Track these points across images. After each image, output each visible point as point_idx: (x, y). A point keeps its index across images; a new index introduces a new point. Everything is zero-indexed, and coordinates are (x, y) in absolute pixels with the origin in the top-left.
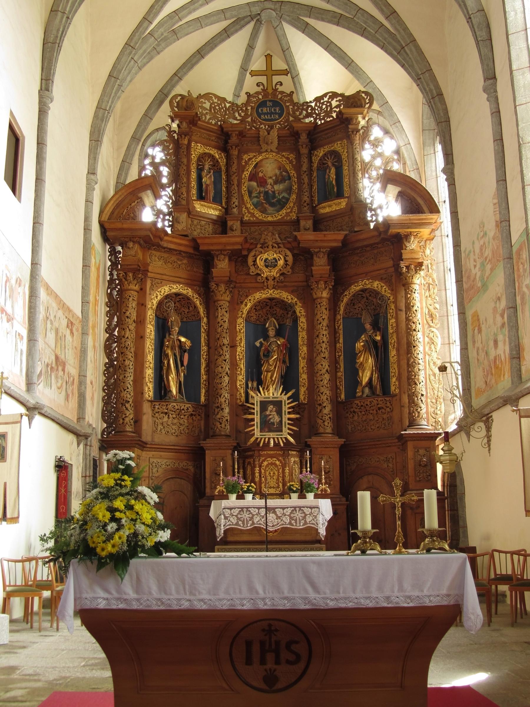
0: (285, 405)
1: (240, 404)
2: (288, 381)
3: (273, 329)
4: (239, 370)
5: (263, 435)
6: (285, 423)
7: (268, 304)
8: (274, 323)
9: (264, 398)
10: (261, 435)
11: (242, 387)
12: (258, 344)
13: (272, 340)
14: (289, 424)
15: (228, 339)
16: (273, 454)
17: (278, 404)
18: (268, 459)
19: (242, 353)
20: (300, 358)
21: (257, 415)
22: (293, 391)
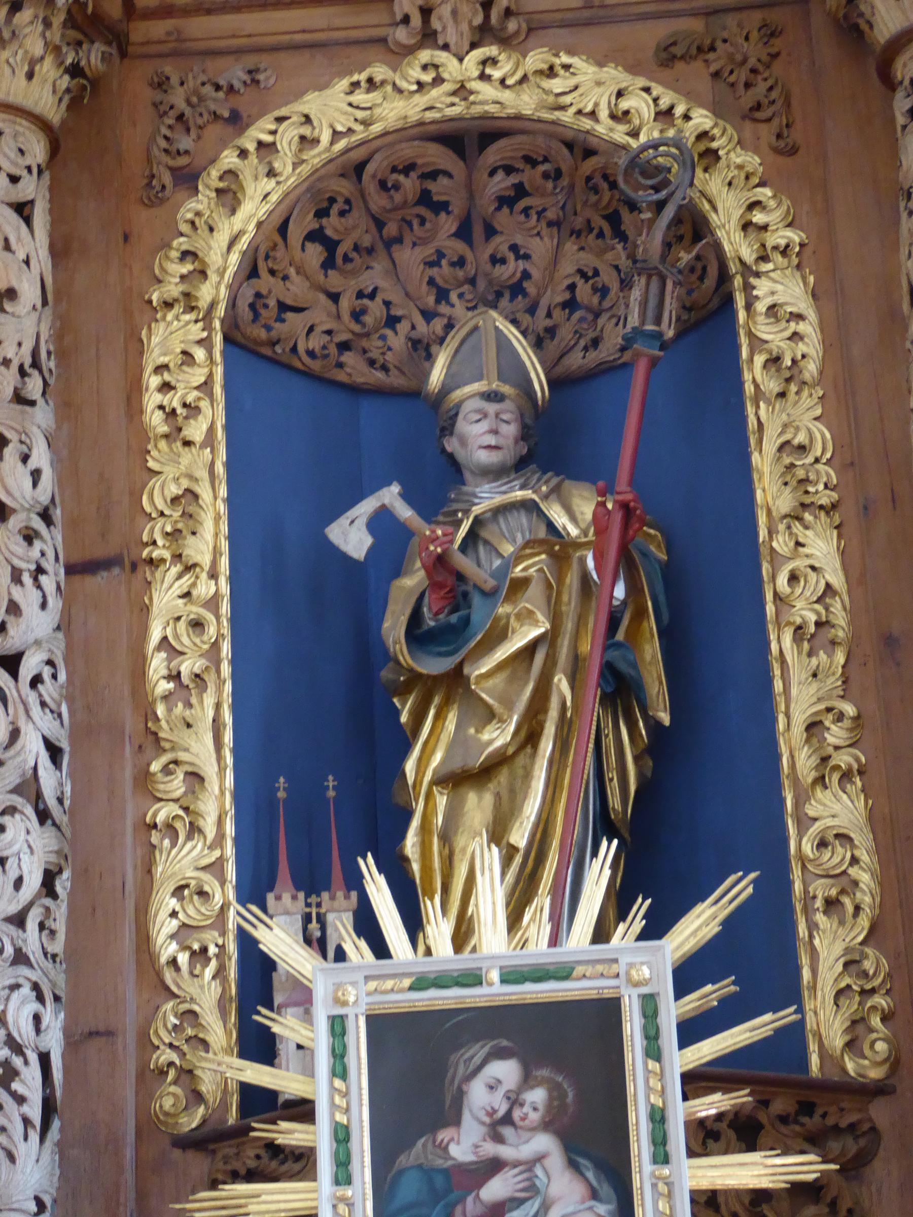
0: (653, 1052)
1: (191, 1121)
2: (676, 812)
3: (492, 397)
4: (177, 785)
7: (439, 188)
8: (502, 343)
9: (421, 983)
12: (352, 536)
13: (487, 497)
15: (41, 457)
17: (576, 1045)
19: (197, 625)
20: (782, 642)
21: (343, 1177)
22: (738, 889)
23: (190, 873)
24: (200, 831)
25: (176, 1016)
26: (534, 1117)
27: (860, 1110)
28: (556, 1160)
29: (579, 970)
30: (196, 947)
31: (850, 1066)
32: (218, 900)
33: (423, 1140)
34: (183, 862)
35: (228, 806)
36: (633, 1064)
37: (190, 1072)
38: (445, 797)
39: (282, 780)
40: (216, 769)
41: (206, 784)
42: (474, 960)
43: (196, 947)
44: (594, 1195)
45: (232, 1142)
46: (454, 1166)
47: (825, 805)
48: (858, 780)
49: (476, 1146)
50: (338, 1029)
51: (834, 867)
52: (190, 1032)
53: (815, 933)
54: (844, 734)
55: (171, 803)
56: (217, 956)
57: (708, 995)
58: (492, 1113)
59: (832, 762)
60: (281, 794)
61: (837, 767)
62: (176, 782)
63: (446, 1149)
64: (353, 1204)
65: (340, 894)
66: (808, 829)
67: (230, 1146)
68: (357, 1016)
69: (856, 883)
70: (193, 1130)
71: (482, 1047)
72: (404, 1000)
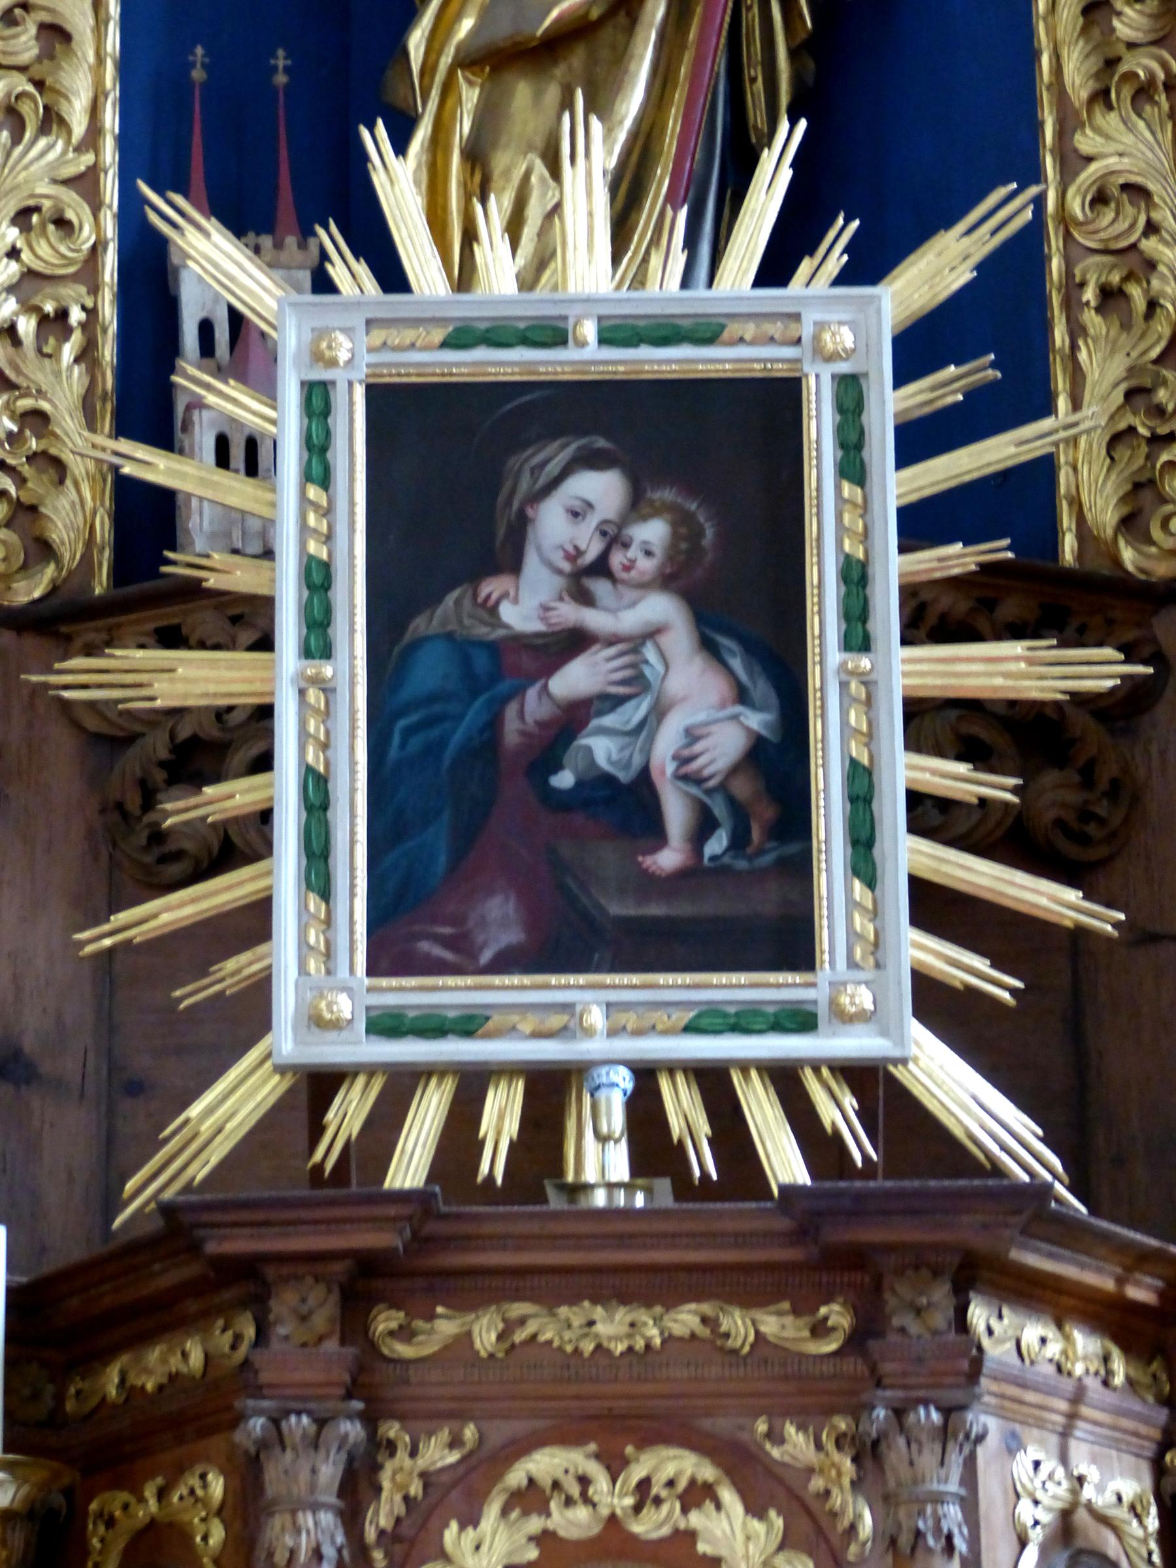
0: (853, 468)
5: (433, 1026)
6: (861, 786)
10: (386, 1025)
11: (55, 324)
14: (930, 815)
16: (641, 1358)
17: (721, 451)
18: (545, 1463)
21: (318, 640)
23: (43, 188)
24: (63, 123)
25: (12, 418)
26: (647, 566)
27: (1138, 625)
28: (680, 637)
29: (733, 329)
30: (49, 308)
31: (1128, 555)
32: (87, 237)
33: (455, 594)
34: (32, 169)
35: (109, 83)
36: (819, 489)
37: (33, 509)
38: (477, 91)
39: (199, 51)
40: (92, 21)
41: (74, 44)
42: (555, 302)
43: (49, 308)
44: (742, 696)
45: (100, 623)
46: (505, 639)
47: (1107, 137)
48: (1162, 98)
49: (546, 608)
50: (317, 402)
51: (1117, 237)
52: (33, 444)
53: (1081, 343)
54: (1143, 21)
55: (15, 74)
56: (84, 326)
57: (945, 386)
58: (574, 555)
59: (1123, 68)
60: (198, 74)
61: (1131, 76)
62: (23, 38)
63: (494, 610)
64: (334, 690)
65: (291, 241)
66: (1076, 174)
67: (97, 630)
68: (350, 384)
69: (1151, 265)
70: (35, 602)
71: (563, 447)
72: (430, 361)
